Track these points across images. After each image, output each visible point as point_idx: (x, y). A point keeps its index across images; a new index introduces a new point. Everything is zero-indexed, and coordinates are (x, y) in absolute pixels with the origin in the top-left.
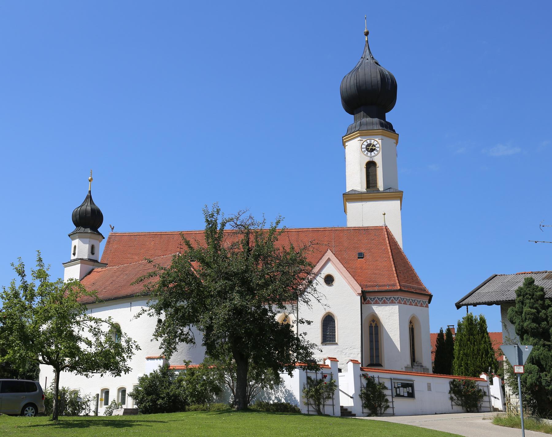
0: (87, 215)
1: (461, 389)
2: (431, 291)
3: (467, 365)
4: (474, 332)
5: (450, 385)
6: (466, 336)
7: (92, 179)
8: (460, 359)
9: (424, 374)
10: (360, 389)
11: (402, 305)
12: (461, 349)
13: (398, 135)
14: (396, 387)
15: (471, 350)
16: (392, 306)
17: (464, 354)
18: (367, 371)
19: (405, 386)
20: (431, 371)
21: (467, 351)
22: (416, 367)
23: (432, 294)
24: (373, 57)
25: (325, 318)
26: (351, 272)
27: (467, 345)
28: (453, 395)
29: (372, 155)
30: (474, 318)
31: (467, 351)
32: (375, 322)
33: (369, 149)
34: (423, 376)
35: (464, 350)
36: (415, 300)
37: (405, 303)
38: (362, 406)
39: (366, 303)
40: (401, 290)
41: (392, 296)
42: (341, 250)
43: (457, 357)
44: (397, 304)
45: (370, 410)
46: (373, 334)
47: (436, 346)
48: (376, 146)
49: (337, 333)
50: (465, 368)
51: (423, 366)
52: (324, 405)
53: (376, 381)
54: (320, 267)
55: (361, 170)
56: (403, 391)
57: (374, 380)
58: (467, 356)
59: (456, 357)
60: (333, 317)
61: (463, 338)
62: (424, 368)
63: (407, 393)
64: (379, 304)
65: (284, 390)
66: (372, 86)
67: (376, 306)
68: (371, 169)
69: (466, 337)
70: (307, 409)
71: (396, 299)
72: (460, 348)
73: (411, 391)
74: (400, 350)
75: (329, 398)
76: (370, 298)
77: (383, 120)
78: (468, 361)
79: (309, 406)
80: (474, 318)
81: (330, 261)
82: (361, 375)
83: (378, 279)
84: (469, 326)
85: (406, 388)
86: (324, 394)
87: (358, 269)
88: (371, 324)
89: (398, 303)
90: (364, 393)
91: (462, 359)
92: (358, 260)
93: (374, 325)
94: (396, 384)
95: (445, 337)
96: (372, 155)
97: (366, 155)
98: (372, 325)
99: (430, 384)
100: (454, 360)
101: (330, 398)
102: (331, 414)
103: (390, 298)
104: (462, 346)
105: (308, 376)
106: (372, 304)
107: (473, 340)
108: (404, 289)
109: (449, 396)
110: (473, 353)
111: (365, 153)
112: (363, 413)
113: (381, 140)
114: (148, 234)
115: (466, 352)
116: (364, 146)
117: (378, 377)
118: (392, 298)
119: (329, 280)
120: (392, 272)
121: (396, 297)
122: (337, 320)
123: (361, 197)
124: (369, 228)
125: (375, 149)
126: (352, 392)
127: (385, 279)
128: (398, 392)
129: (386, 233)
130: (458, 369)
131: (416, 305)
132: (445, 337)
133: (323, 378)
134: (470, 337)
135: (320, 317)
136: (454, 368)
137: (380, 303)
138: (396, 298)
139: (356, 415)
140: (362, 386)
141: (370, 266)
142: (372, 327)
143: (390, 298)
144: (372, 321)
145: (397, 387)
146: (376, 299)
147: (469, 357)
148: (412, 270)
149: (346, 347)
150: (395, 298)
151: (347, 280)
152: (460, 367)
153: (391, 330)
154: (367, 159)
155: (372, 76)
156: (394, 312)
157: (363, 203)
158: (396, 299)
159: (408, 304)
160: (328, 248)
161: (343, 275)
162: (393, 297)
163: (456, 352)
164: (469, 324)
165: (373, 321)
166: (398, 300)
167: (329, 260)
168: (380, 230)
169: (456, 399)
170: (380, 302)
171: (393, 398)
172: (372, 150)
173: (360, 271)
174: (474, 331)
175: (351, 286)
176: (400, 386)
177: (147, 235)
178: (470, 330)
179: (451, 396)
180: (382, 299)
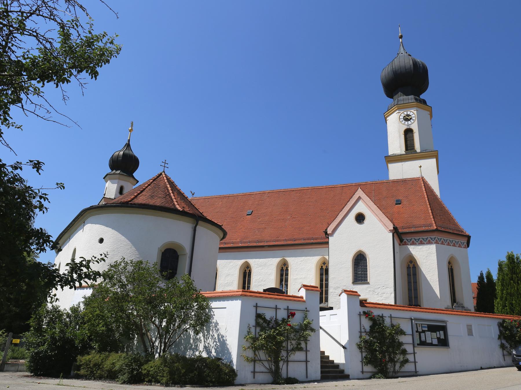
0: (119, 159)
2: (468, 233)
4: (517, 271)
5: (499, 327)
6: (509, 275)
7: (132, 129)
8: (504, 299)
9: (461, 312)
10: (359, 334)
11: (440, 245)
12: (504, 288)
13: (431, 108)
14: (419, 331)
17: (507, 294)
18: (372, 307)
19: (433, 328)
20: (473, 310)
21: (511, 291)
23: (470, 235)
24: (406, 52)
25: (357, 257)
26: (389, 217)
27: (511, 284)
28: (504, 342)
30: (515, 257)
31: (511, 291)
32: (412, 263)
34: (460, 315)
35: (508, 289)
37: (442, 243)
38: (362, 362)
39: (403, 245)
41: (429, 236)
43: (500, 297)
45: (375, 367)
46: (411, 275)
47: (477, 289)
49: (369, 271)
50: (510, 308)
51: (465, 307)
52: (288, 361)
53: (387, 322)
54: (351, 206)
55: (400, 137)
56: (430, 337)
57: (383, 321)
58: (511, 296)
59: (499, 297)
60: (364, 255)
61: (505, 277)
62: (465, 308)
63: (437, 340)
65: (216, 336)
66: (406, 70)
69: (508, 276)
70: (252, 370)
72: (503, 288)
73: (442, 337)
75: (298, 348)
76: (406, 239)
77: (418, 97)
78: (513, 301)
79: (256, 364)
80: (515, 257)
81: (361, 199)
82: (360, 312)
83: (414, 221)
84: (510, 265)
85: (435, 332)
86: (289, 344)
88: (409, 265)
89: (435, 243)
90: (366, 342)
91: (505, 299)
92: (396, 206)
93: (411, 266)
94: (419, 327)
95: (485, 280)
97: (404, 124)
98: (410, 266)
100: (497, 300)
101: (301, 349)
102: (303, 378)
104: (504, 286)
105: (258, 313)
107: (516, 279)
109: (499, 343)
110: (518, 292)
111: (403, 123)
112: (363, 372)
113: (416, 111)
114: (220, 196)
115: (509, 291)
117: (391, 317)
118: (429, 239)
119: (360, 218)
121: (433, 237)
122: (369, 258)
123: (400, 159)
124: (406, 180)
125: (411, 118)
126: (344, 339)
128: (423, 339)
129: (422, 182)
131: (454, 245)
132: (485, 280)
133: (288, 317)
134: (513, 276)
135: (351, 256)
137: (417, 243)
138: (433, 238)
139: (350, 377)
140: (363, 330)
142: (410, 268)
144: (410, 262)
145: (421, 331)
146: (413, 240)
147: (513, 297)
149: (379, 286)
151: (379, 217)
152: (504, 308)
153: (429, 270)
154: (405, 127)
155: (406, 62)
157: (403, 163)
158: (433, 239)
159: (446, 244)
160: (358, 187)
161: (374, 213)
162: (430, 238)
163: (499, 292)
164: (511, 263)
165: (411, 262)
166: (435, 240)
167: (359, 198)
169: (509, 346)
171: (415, 348)
173: (397, 215)
174: (517, 270)
176: (426, 329)
177: (218, 197)
178: (512, 269)
179: (501, 343)
180: (419, 240)
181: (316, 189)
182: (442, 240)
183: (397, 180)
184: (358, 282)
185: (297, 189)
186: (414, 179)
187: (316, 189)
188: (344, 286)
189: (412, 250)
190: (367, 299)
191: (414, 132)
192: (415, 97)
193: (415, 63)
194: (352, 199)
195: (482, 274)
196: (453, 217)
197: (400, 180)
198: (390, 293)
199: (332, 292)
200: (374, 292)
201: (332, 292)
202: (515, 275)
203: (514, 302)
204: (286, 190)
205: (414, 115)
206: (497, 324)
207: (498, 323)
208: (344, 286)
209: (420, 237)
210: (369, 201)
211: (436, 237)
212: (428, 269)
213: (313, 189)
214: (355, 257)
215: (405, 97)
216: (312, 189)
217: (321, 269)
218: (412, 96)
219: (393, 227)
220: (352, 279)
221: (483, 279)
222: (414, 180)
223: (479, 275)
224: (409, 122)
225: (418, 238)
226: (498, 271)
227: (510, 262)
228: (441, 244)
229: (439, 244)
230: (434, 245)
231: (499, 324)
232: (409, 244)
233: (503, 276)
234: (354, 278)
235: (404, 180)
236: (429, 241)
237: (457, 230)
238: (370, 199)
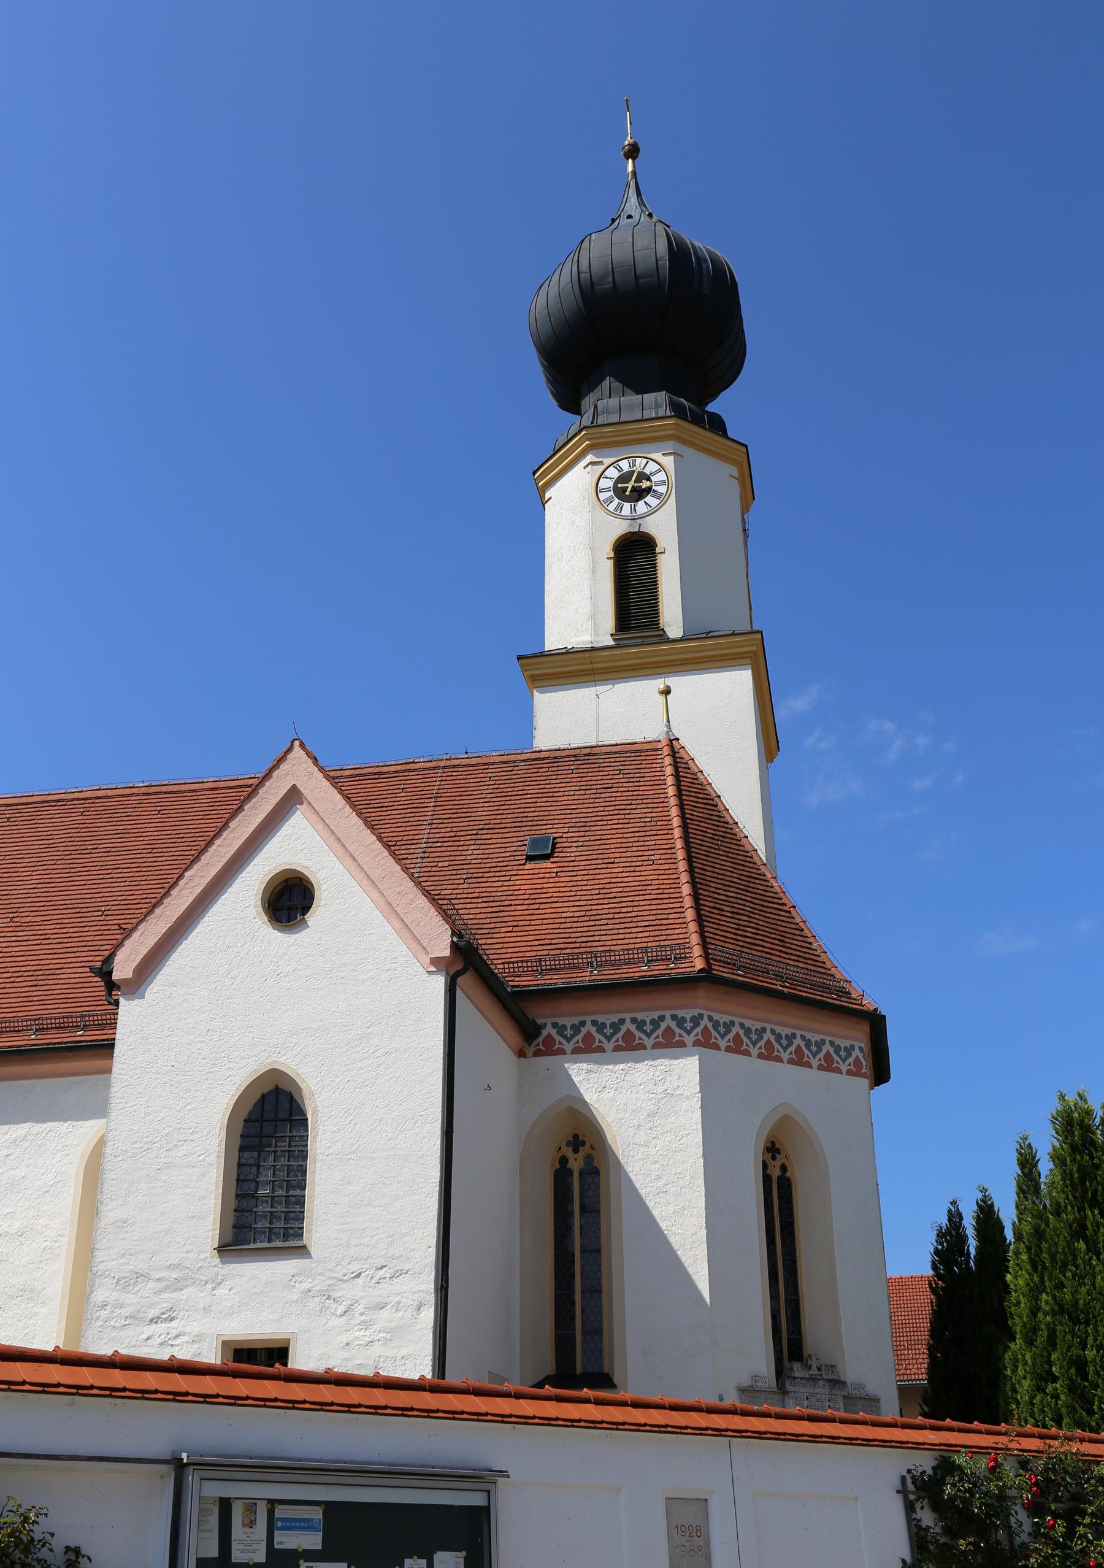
1: (1018, 1541)
3: (1082, 1371)
5: (910, 1508)
8: (1042, 1337)
11: (721, 1056)
15: (1093, 1284)
16: (666, 1062)
17: (1060, 1309)
21: (1075, 1293)
22: (803, 1390)
27: (1075, 1259)
29: (638, 513)
33: (625, 490)
34: (868, 1442)
35: (1060, 1286)
36: (791, 1038)
37: (736, 1048)
39: (537, 1054)
40: (706, 978)
42: (458, 834)
43: (1025, 1325)
44: (690, 1048)
47: (934, 1291)
48: (654, 478)
50: (1072, 1388)
51: (844, 1383)
55: (594, 570)
58: (1077, 1322)
60: (296, 1097)
61: (1047, 1225)
62: (851, 1390)
66: (636, 277)
67: (584, 1066)
68: (638, 562)
71: (688, 1025)
72: (1036, 1278)
74: (706, 1294)
76: (554, 1025)
78: (1084, 1348)
83: (603, 938)
84: (1073, 1160)
87: (518, 902)
88: (564, 1160)
89: (696, 1043)
93: (576, 1164)
94: (251, 1524)
95: (972, 1244)
96: (638, 513)
97: (617, 514)
99: (706, 1500)
100: (1012, 1346)
103: (656, 1024)
104: (1045, 1268)
106: (569, 1056)
108: (725, 975)
111: (612, 507)
113: (671, 458)
116: (605, 483)
120: (679, 905)
121: (688, 1014)
123: (589, 666)
125: (649, 490)
127: (640, 935)
129: (668, 760)
130: (1032, 1397)
131: (799, 1060)
132: (972, 1244)
134: (1086, 1216)
136: (1015, 1391)
138: (688, 1018)
141: (574, 889)
142: (570, 1172)
143: (656, 1024)
146: (589, 1028)
147: (1087, 1324)
148: (784, 908)
149: (355, 1267)
150: (680, 1022)
153: (661, 1183)
154: (619, 528)
155: (639, 245)
157: (601, 689)
158: (688, 1025)
159: (755, 1051)
163: (1018, 1303)
164: (1074, 1149)
165: (576, 1143)
167: (293, 798)
168: (643, 754)
172: (639, 494)
173: (525, 907)
175: (321, 826)
181: (166, 793)
182: (736, 1029)
183: (553, 754)
184: (252, 1246)
185: (76, 796)
186: (635, 747)
187: (166, 793)
188: (170, 1268)
189: (582, 1077)
190: (225, 1344)
191: (658, 550)
192: (671, 400)
193: (679, 252)
194: (254, 800)
195: (955, 1218)
196: (801, 924)
197: (567, 753)
198: (416, 1304)
199: (104, 1306)
200: (329, 1298)
201: (104, 1306)
202: (1096, 1212)
203: (1090, 1354)
204: (24, 800)
205: (661, 476)
206: (898, 1485)
207: (903, 1479)
208: (170, 1268)
210: (343, 808)
211: (701, 1016)
212: (659, 1177)
213: (155, 794)
214: (249, 1106)
215: (634, 398)
216: (147, 794)
218: (662, 396)
219: (454, 946)
220: (218, 1226)
221: (962, 1239)
222: (630, 752)
223: (944, 1221)
225: (615, 1018)
226: (1018, 1194)
227: (1071, 1146)
228: (728, 1049)
229: (720, 1049)
231: (910, 1487)
232: (649, 1045)
233: (1039, 1216)
234: (231, 1221)
235: (588, 751)
237: (814, 986)
238: (343, 802)
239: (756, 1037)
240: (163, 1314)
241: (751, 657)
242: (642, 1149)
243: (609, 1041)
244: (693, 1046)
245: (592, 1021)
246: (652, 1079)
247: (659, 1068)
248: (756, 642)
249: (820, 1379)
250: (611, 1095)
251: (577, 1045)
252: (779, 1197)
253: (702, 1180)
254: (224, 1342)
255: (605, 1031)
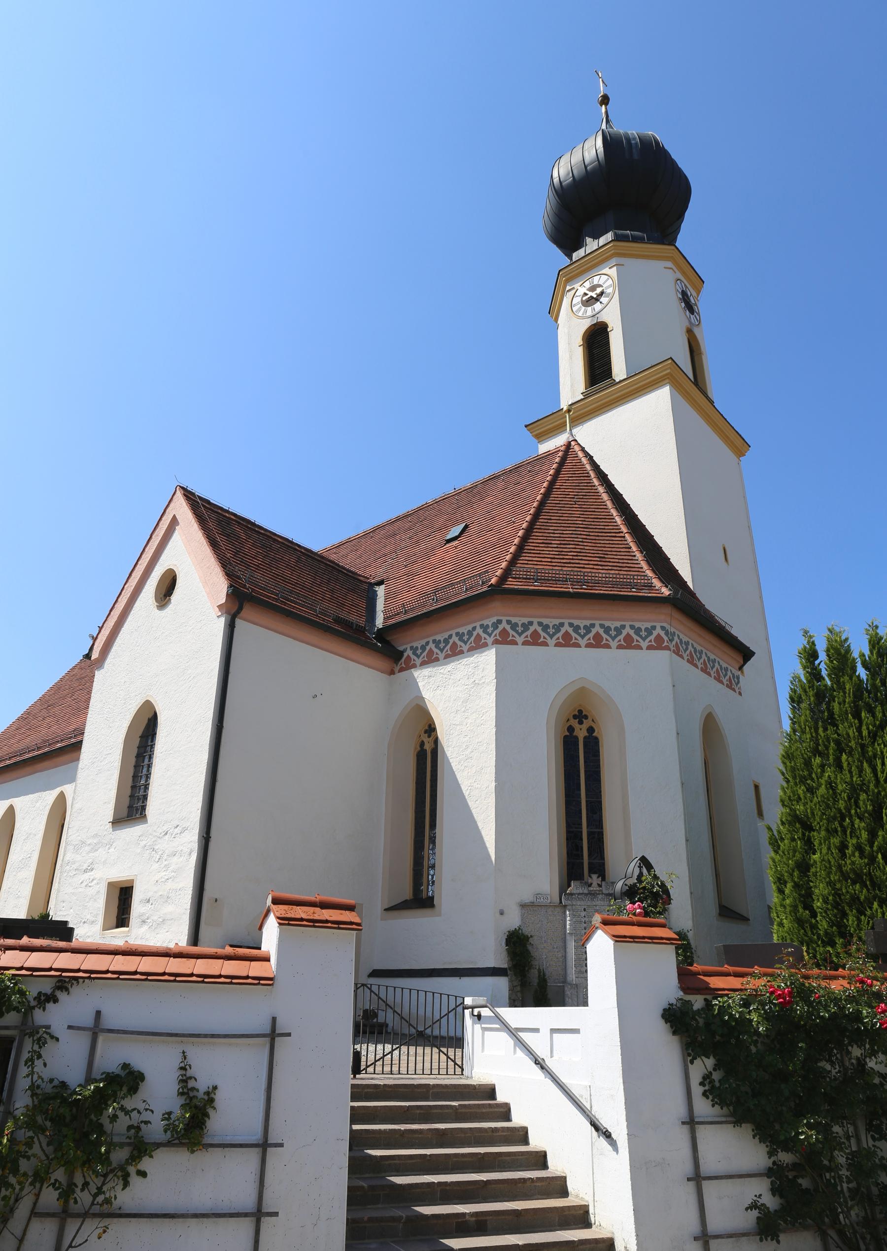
41: (464, 624)
64: (516, 644)
66: (586, 167)
88: (571, 729)
89: (496, 642)
93: (581, 733)
143: (619, 631)
144: (575, 717)
153: (467, 752)
155: (575, 172)
156: (480, 680)
165: (580, 716)
170: (549, 640)
190: (133, 880)
209: (474, 625)
217: (565, 737)
224: (598, 306)
229: (580, 647)
230: (492, 648)
232: (465, 651)
236: (535, 635)
239: (554, 631)
240: (89, 866)
241: (668, 378)
242: (458, 728)
243: (613, 640)
244: (492, 644)
245: (538, 622)
246: (467, 674)
247: (471, 666)
248: (669, 366)
249: (599, 894)
250: (442, 691)
251: (527, 639)
252: (585, 752)
253: (494, 745)
254: (109, 884)
255: (580, 631)
